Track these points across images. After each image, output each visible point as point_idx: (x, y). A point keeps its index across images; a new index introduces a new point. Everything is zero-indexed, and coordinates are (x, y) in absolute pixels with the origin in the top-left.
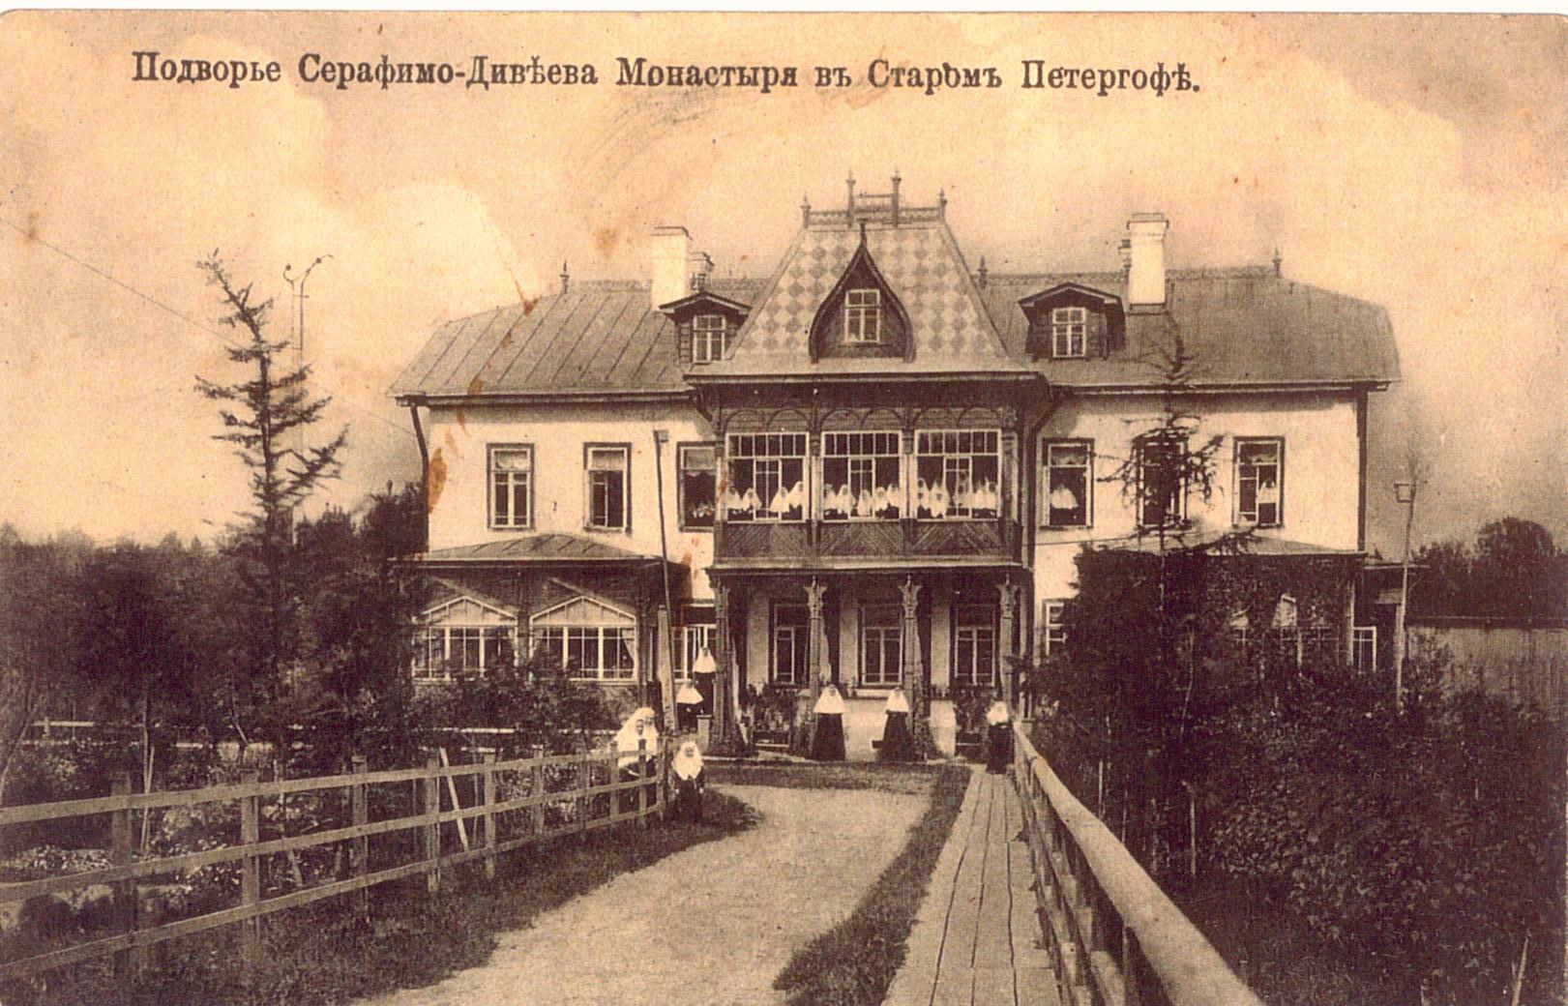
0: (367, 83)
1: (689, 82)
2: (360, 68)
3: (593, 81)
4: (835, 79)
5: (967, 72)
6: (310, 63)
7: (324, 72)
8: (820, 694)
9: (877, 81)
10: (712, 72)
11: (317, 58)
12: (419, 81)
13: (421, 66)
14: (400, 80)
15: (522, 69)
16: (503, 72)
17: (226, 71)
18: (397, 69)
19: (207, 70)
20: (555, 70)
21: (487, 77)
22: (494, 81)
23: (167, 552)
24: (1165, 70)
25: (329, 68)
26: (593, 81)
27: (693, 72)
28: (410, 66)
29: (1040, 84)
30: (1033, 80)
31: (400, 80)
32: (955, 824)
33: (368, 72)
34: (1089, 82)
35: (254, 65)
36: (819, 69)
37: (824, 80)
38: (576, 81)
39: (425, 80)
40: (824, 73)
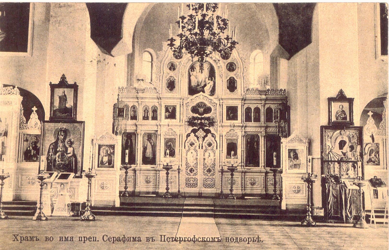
0: (119, 242)
1: (70, 240)
2: (118, 238)
3: (140, 241)
4: (151, 240)
5: (212, 238)
6: (105, 237)
7: (109, 239)
8: (48, 30)
9: (105, 240)
10: (168, 238)
11: (107, 236)
12: (65, 241)
13: (133, 238)
14: (128, 241)
15: (149, 238)
16: (130, 239)
17: (246, 240)
18: (127, 238)
19: (48, 239)
20: (90, 238)
21: (238, 241)
22: (240, 241)
23: (85, 62)
24: (125, 236)
25: (110, 238)
26: (140, 241)
27: (139, 238)
28: (82, 237)
29: (164, 241)
30: (163, 240)
31: (128, 241)
32: (320, 83)
33: (120, 239)
34: (90, 240)
35: (253, 238)
36: (147, 238)
37: (148, 240)
38: (48, 240)
39: (134, 241)
40: (148, 238)
